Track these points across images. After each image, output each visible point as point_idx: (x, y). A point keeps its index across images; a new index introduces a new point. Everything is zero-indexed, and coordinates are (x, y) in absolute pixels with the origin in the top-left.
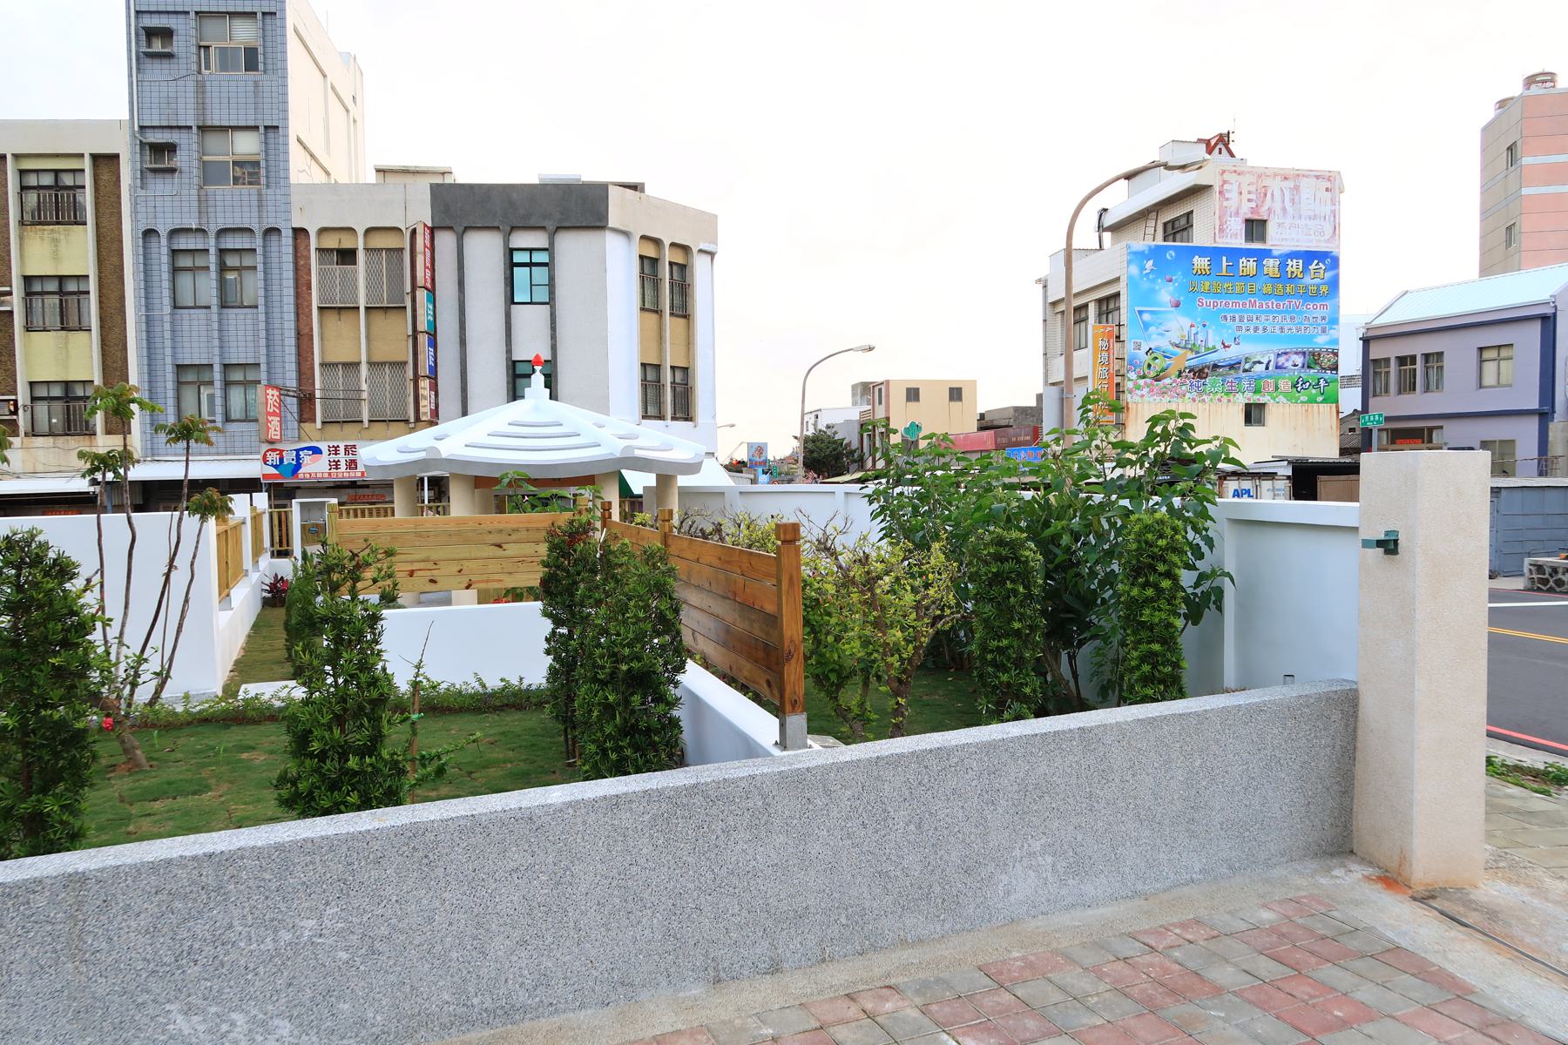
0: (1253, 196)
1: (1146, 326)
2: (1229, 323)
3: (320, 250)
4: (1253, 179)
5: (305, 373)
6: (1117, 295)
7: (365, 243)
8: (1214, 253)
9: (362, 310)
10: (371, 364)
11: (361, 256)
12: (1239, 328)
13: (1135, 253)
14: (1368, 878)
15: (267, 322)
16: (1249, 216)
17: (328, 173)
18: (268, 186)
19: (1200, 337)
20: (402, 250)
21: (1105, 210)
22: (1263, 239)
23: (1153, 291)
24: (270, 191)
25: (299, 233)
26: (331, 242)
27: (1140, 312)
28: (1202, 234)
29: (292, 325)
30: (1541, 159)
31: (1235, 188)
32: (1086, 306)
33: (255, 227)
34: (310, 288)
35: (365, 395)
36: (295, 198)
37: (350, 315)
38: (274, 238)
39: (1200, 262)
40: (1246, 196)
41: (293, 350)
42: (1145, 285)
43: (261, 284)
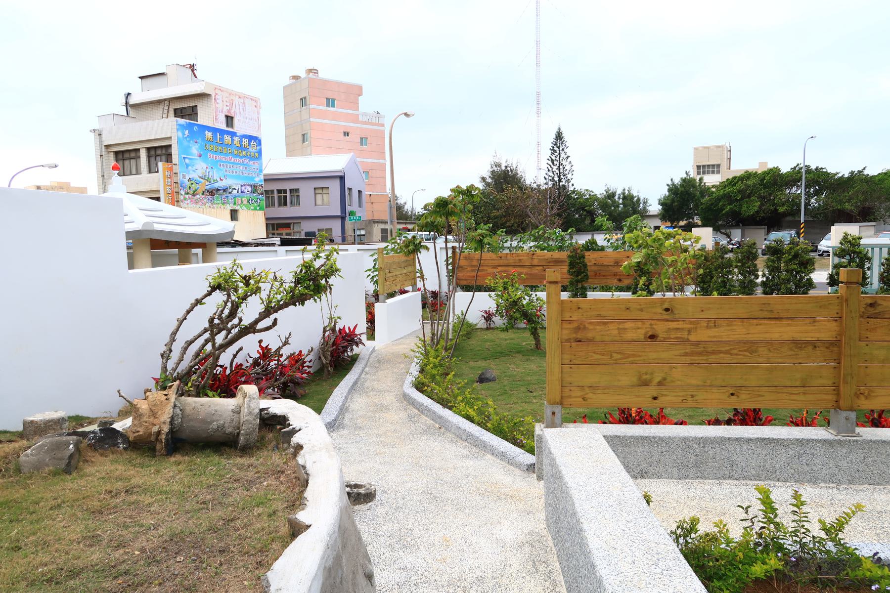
1: (187, 166)
8: (215, 130)
13: (180, 125)
22: (232, 127)
23: (189, 147)
32: (138, 150)
39: (209, 134)
42: (185, 143)
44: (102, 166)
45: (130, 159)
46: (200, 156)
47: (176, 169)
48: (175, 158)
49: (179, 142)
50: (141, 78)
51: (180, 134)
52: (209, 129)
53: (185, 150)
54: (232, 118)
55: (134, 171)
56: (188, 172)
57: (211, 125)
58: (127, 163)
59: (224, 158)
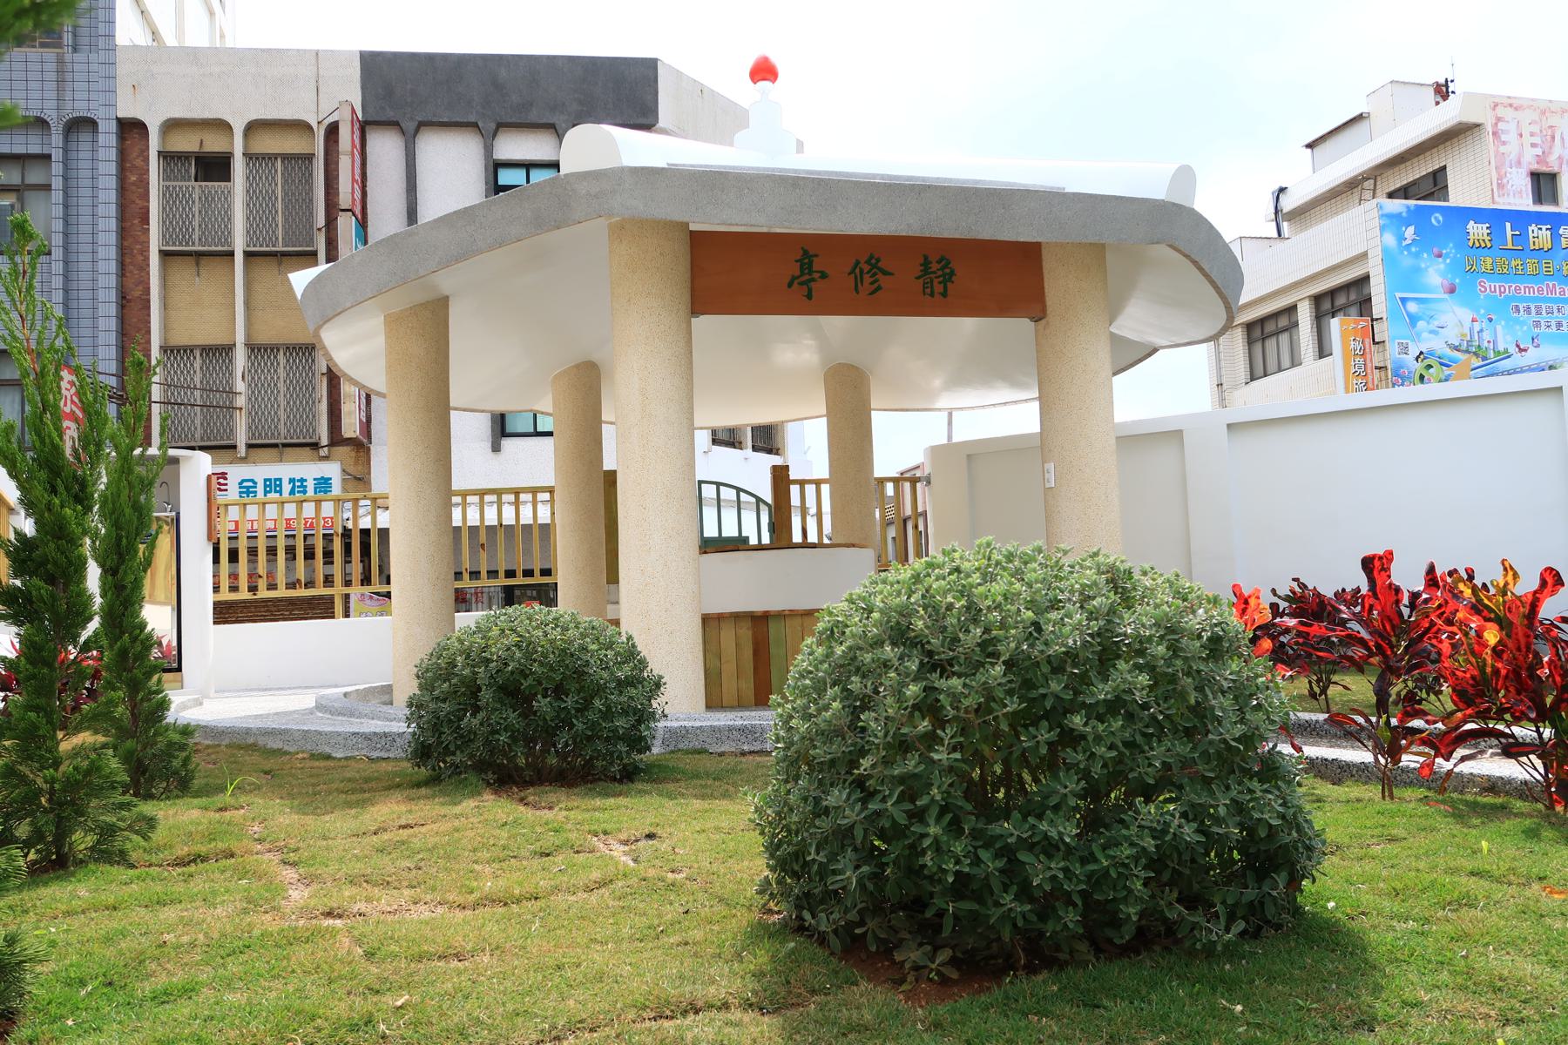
0: (1537, 140)
1: (1413, 320)
2: (1523, 315)
3: (164, 155)
4: (1535, 116)
5: (132, 364)
6: (1365, 280)
7: (246, 146)
8: (1495, 218)
9: (239, 258)
10: (253, 348)
11: (239, 167)
12: (1537, 324)
13: (1390, 216)
15: (66, 277)
16: (1535, 167)
18: (75, 50)
19: (1486, 336)
20: (310, 157)
21: (1282, 190)
22: (1555, 200)
23: (1417, 270)
24: (78, 57)
25: (131, 129)
26: (186, 143)
27: (1404, 300)
28: (1464, 190)
29: (112, 281)
31: (1512, 127)
32: (1292, 309)
33: (50, 115)
34: (145, 219)
35: (241, 401)
36: (123, 70)
37: (216, 266)
38: (85, 137)
39: (1477, 230)
40: (1527, 140)
41: (113, 324)
42: (1407, 261)
43: (58, 211)
44: (1219, 360)
45: (1277, 333)
46: (1452, 290)
47: (1381, 332)
48: (1379, 307)
49: (1388, 258)
50: (1310, 146)
51: (1390, 239)
52: (1477, 214)
53: (1407, 280)
54: (1553, 177)
55: (1286, 362)
56: (1417, 338)
57: (1485, 204)
58: (1271, 344)
59: (1529, 290)
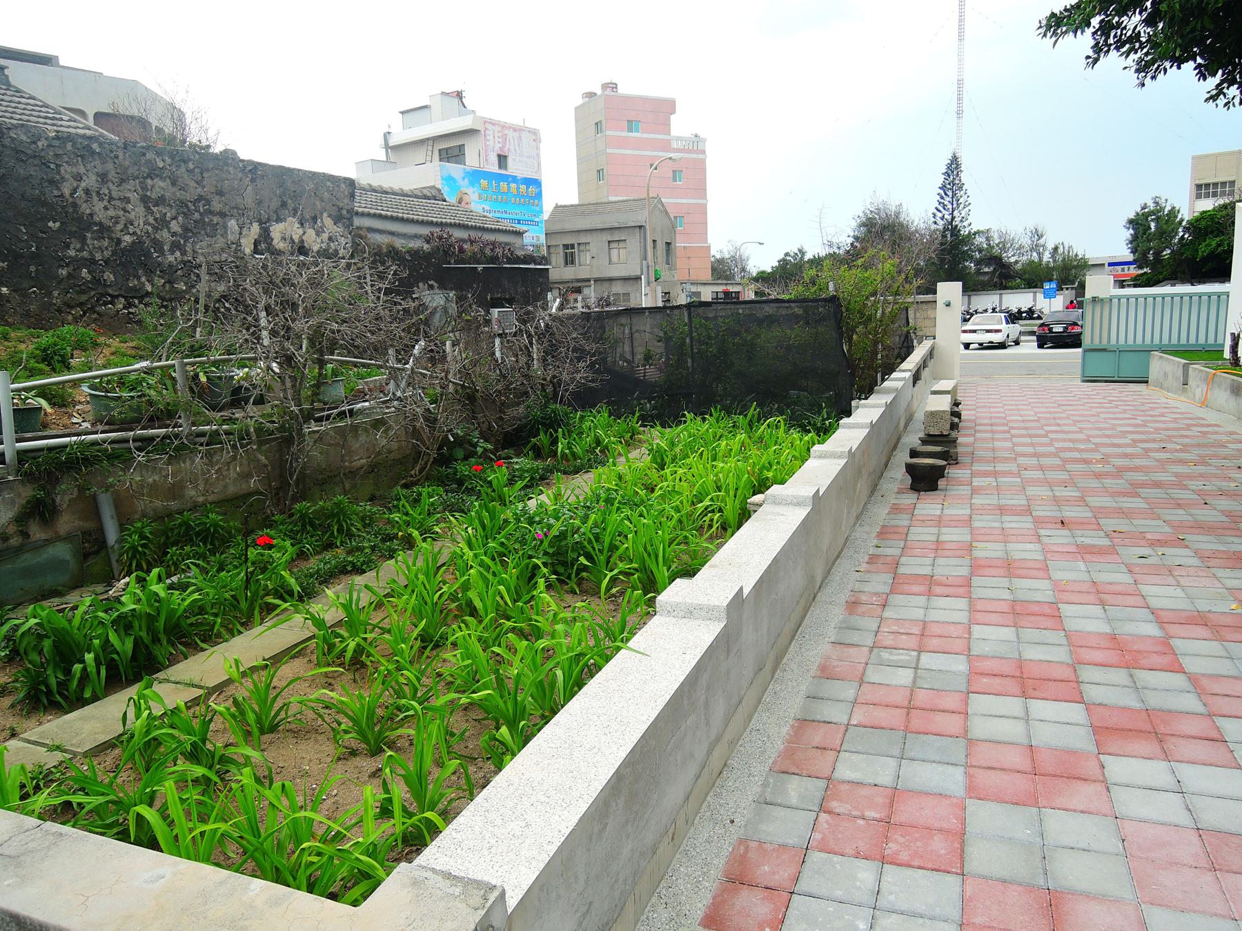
14: (741, 589)
17: (1131, 676)
30: (614, 133)
